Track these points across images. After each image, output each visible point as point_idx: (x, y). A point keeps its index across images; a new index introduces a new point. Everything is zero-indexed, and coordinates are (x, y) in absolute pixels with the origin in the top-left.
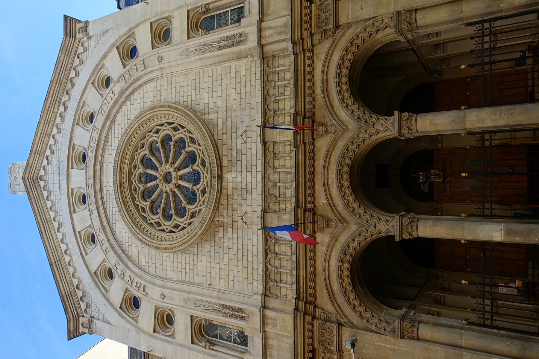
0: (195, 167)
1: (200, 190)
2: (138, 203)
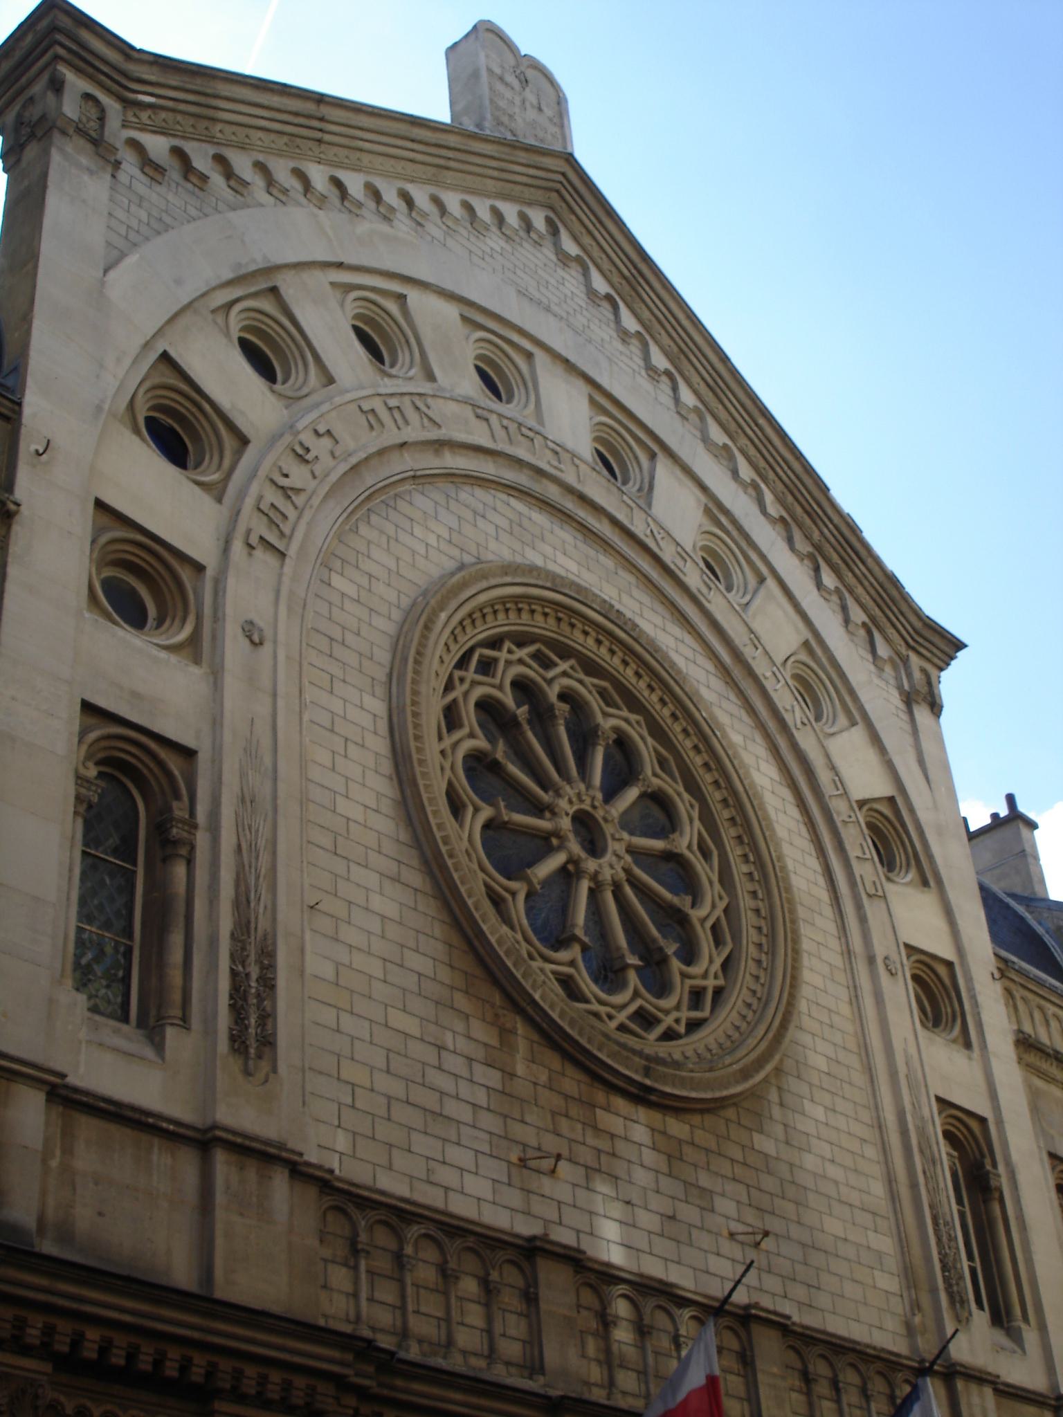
0: (520, 888)
1: (470, 809)
2: (633, 717)
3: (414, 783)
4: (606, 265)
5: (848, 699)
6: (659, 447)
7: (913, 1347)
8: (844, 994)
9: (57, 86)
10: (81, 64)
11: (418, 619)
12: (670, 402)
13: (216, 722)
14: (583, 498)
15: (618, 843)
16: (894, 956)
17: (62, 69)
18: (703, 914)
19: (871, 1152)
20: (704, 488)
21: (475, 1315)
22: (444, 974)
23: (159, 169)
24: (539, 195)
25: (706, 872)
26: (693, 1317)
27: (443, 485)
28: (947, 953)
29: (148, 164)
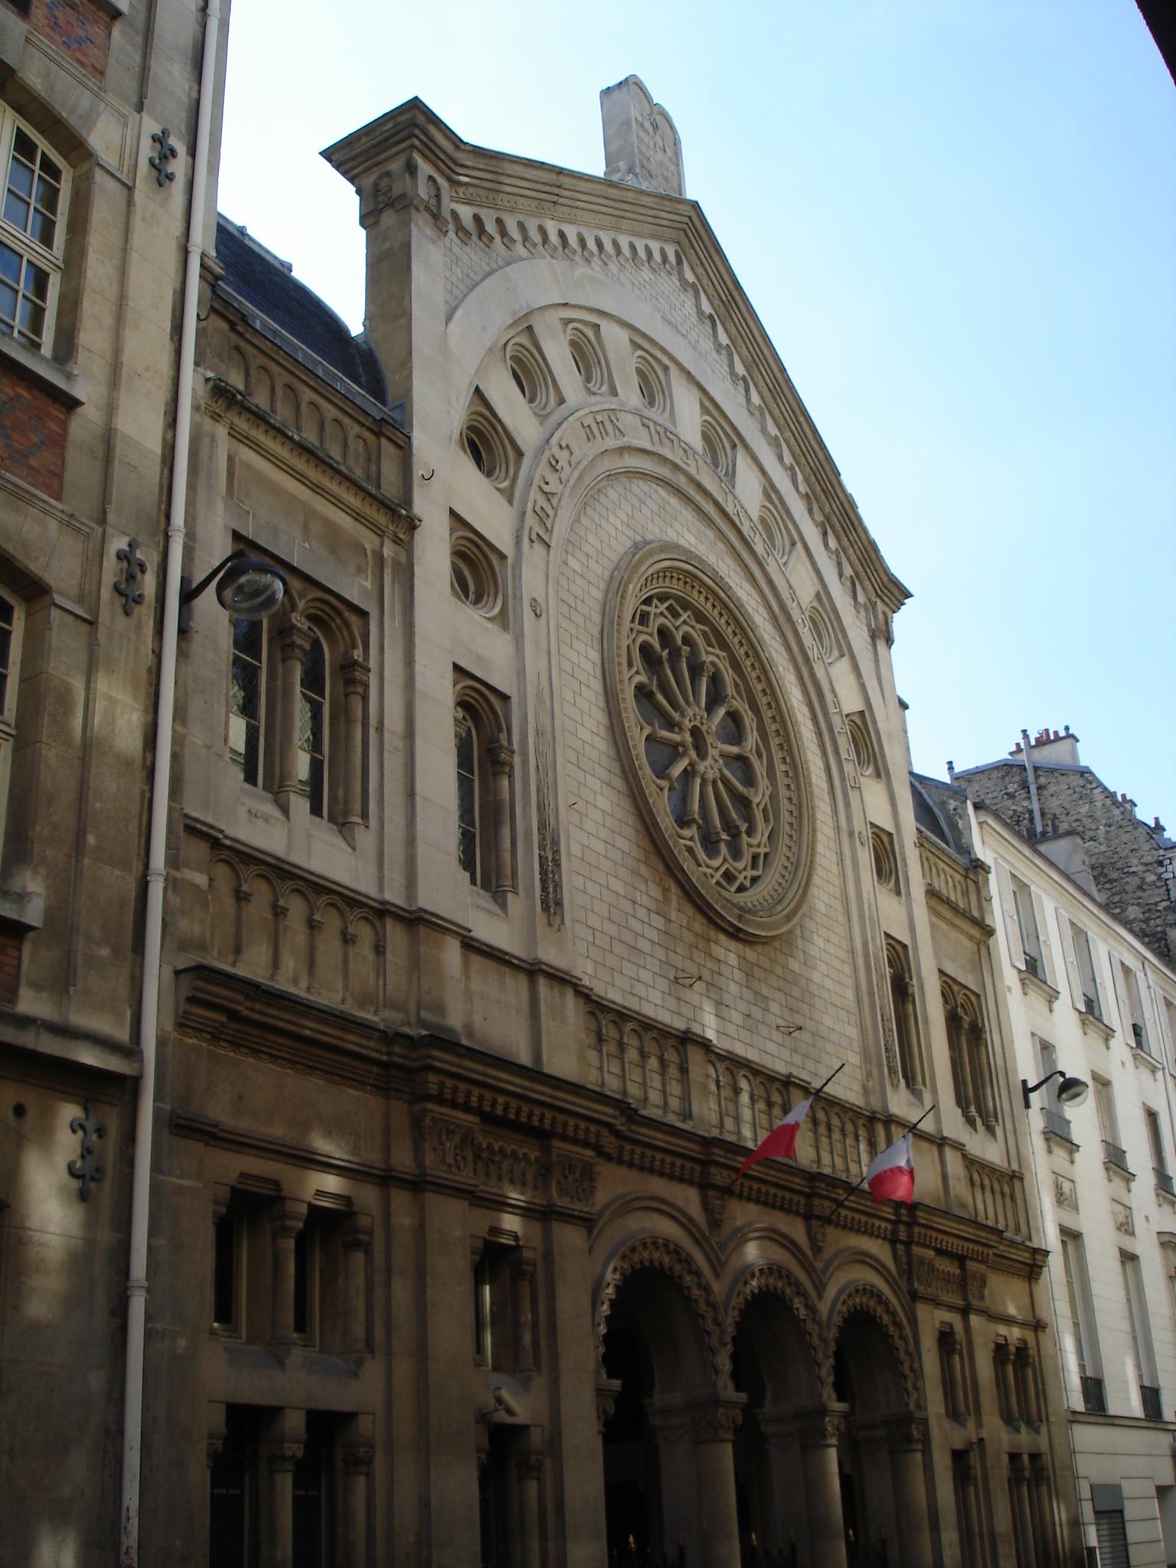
3: (619, 715)
4: (711, 291)
5: (840, 636)
6: (739, 440)
7: (868, 1102)
8: (834, 858)
9: (411, 169)
10: (428, 152)
11: (615, 588)
12: (742, 400)
13: (521, 674)
14: (699, 486)
15: (717, 748)
16: (864, 832)
17: (417, 157)
18: (759, 797)
19: (847, 969)
20: (763, 472)
21: (656, 1081)
22: (635, 852)
23: (468, 234)
24: (672, 234)
25: (759, 768)
26: (633, 1030)
27: (623, 480)
28: (890, 828)
29: (460, 228)
